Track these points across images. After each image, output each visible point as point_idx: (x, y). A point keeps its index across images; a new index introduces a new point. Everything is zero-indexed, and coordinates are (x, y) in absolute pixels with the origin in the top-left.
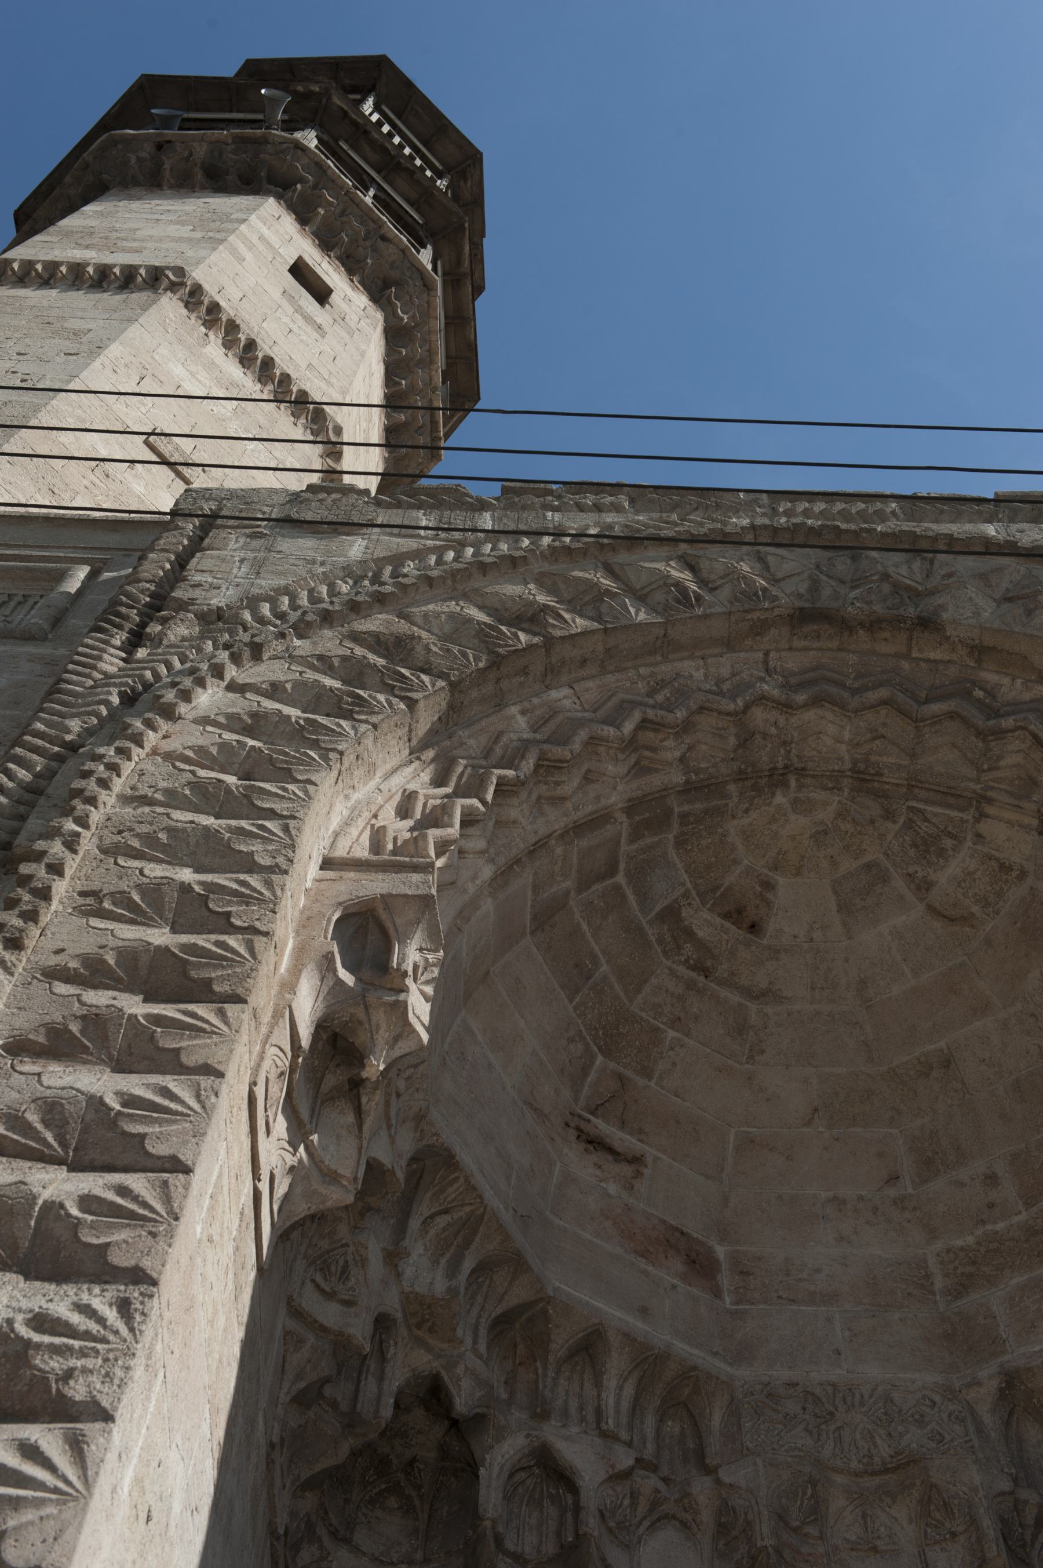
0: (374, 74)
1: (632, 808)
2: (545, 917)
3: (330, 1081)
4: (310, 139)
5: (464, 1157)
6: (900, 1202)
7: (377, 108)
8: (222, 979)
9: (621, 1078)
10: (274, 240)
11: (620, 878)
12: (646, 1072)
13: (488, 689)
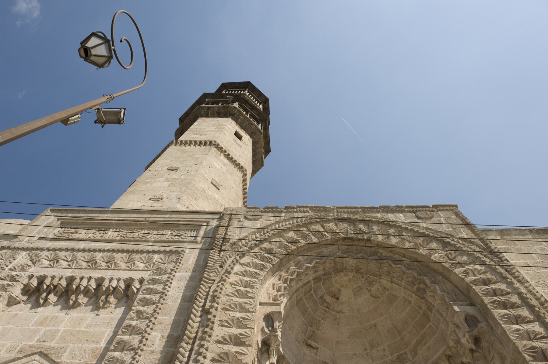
0: (248, 85)
1: (314, 280)
2: (298, 303)
3: (264, 349)
4: (236, 105)
5: (287, 356)
6: (367, 354)
7: (248, 92)
8: (247, 341)
9: (313, 331)
10: (231, 128)
11: (312, 292)
12: (318, 330)
13: (287, 258)
